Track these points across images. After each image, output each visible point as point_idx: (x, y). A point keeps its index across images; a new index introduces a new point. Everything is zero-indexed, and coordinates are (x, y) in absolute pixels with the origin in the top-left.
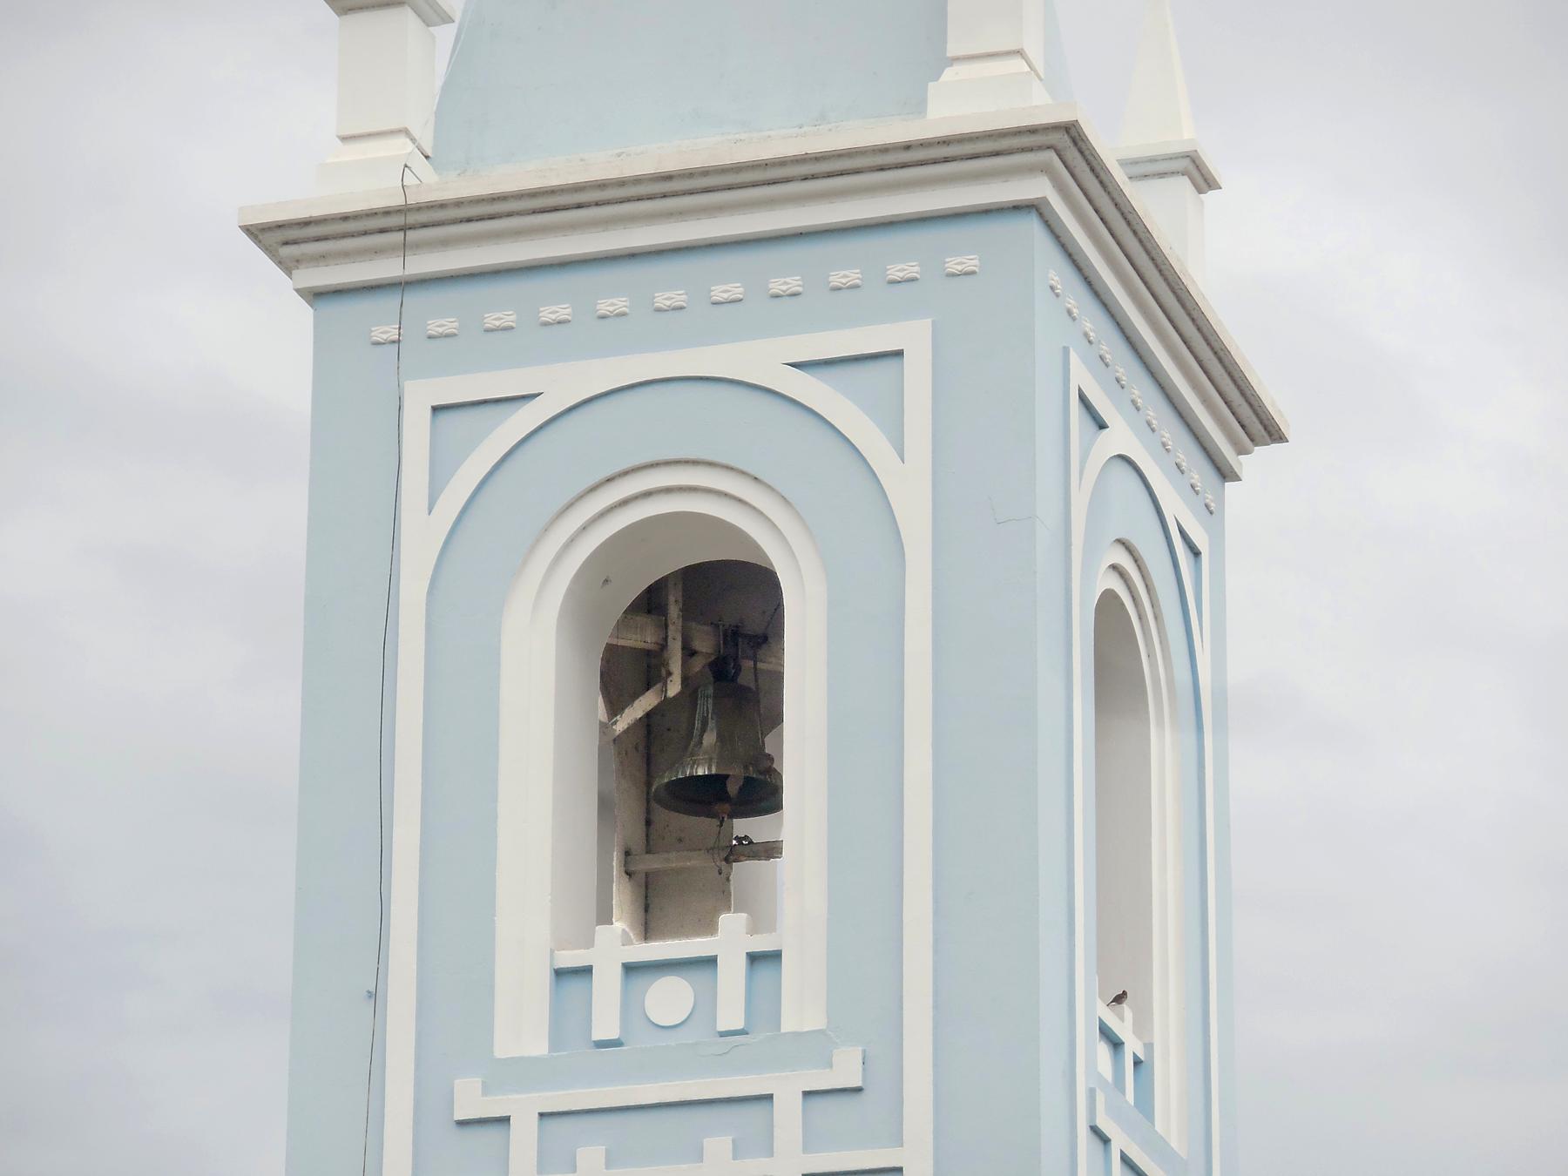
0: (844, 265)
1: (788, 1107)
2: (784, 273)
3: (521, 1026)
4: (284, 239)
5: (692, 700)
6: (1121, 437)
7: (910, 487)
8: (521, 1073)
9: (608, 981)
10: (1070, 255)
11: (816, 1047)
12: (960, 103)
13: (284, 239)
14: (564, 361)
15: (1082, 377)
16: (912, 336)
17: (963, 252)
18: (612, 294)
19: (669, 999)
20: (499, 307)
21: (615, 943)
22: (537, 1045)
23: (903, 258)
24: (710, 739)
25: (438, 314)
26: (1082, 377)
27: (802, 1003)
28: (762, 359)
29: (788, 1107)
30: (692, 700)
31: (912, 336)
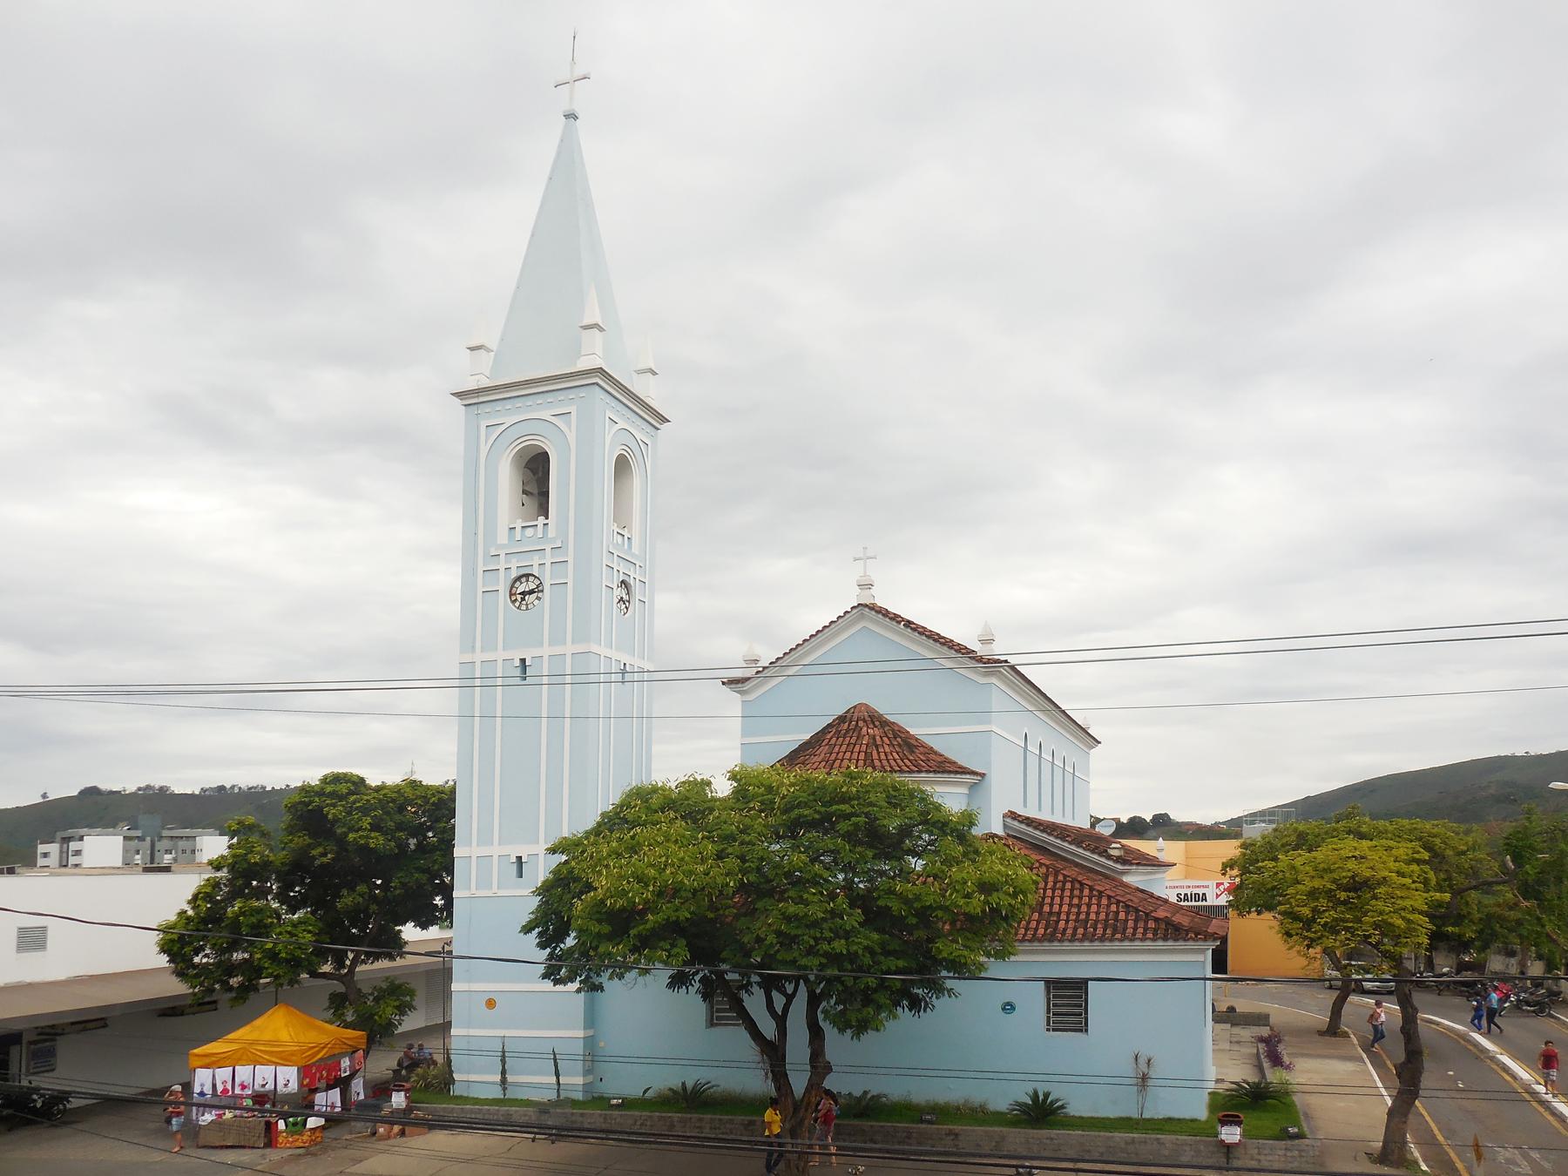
0: (561, 396)
1: (548, 550)
2: (550, 398)
3: (502, 537)
4: (458, 395)
5: (535, 469)
6: (622, 424)
7: (572, 437)
8: (502, 546)
9: (518, 529)
10: (67, 693)
11: (554, 539)
12: (583, 364)
13: (458, 395)
14: (509, 416)
15: (609, 414)
16: (573, 409)
17: (582, 393)
18: (519, 403)
19: (530, 532)
20: (498, 406)
21: (519, 524)
22: (506, 542)
23: (572, 394)
24: (573, 935)
25: (487, 408)
26: (609, 414)
27: (551, 532)
28: (546, 415)
29: (548, 550)
30: (535, 469)
31: (573, 409)
